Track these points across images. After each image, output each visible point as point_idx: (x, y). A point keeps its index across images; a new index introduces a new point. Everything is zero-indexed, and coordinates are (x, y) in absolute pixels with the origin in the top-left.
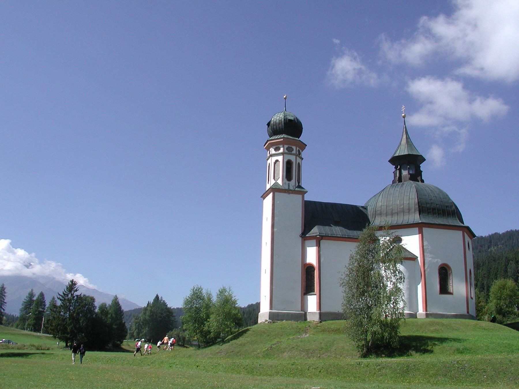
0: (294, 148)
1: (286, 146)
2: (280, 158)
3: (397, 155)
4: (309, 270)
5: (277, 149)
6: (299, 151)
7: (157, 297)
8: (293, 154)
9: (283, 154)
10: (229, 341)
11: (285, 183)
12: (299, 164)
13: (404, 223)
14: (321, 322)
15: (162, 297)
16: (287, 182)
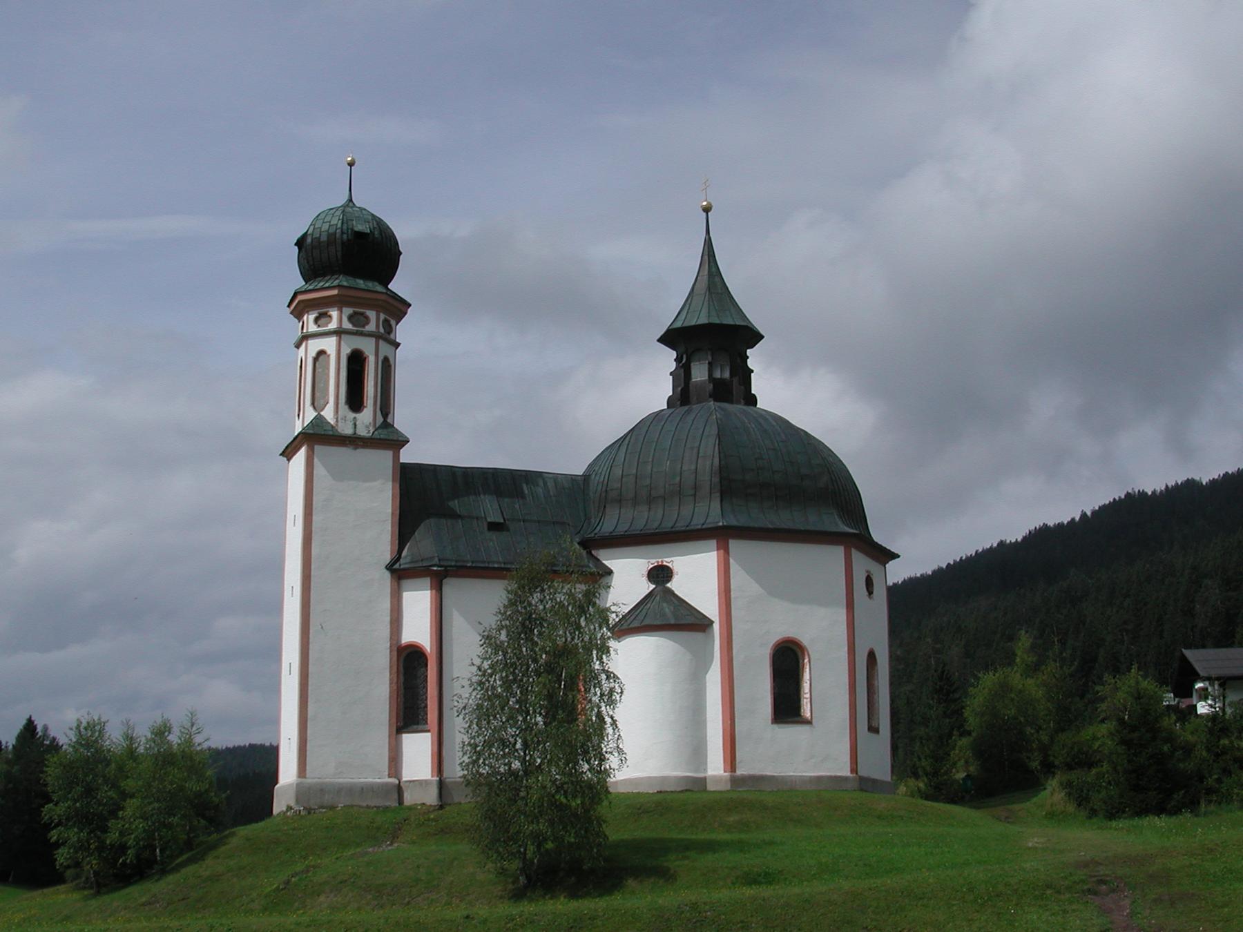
0: (371, 314)
1: (348, 311)
2: (329, 344)
3: (678, 324)
4: (410, 662)
5: (322, 317)
6: (386, 322)
7: (30, 726)
8: (369, 335)
9: (339, 333)
10: (177, 869)
11: (345, 419)
12: (386, 360)
13: (681, 526)
14: (441, 807)
15: (46, 728)
16: (352, 415)
